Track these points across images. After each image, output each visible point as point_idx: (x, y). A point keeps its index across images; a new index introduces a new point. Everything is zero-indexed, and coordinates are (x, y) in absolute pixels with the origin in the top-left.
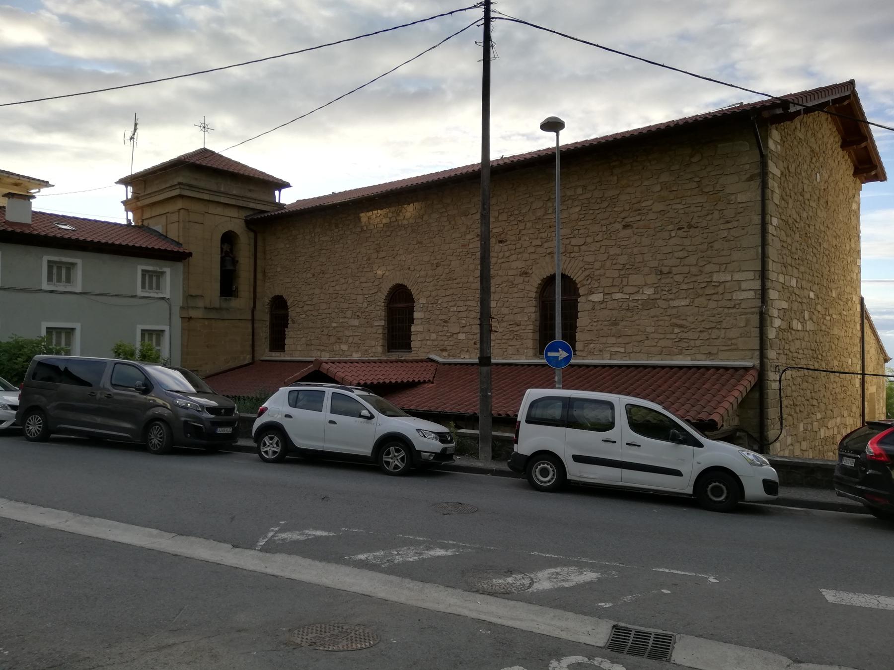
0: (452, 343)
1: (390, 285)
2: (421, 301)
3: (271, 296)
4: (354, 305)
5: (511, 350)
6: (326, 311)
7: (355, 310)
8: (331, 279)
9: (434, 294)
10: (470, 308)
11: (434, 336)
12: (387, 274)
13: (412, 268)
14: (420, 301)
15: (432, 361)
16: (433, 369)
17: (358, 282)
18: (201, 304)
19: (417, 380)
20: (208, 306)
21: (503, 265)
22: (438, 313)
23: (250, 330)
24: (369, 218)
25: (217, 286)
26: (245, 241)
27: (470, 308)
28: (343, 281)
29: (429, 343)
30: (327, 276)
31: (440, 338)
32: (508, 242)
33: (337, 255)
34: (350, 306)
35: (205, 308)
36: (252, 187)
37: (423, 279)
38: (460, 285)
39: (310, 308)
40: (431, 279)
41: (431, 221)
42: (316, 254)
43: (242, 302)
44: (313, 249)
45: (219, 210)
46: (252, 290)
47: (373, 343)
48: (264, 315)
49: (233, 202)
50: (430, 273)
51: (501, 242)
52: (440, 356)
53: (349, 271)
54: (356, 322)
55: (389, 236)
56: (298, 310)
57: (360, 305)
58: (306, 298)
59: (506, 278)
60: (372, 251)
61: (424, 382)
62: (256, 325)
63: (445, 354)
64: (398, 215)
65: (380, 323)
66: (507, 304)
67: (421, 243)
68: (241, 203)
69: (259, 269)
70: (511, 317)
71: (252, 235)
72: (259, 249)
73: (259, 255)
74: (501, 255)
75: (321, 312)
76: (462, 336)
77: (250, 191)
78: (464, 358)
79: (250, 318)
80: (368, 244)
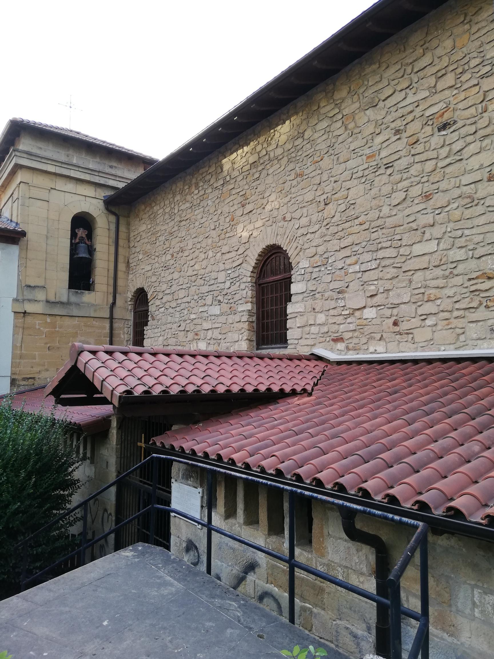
0: (352, 327)
1: (259, 250)
2: (301, 265)
3: (133, 290)
4: (214, 287)
5: (473, 331)
6: (185, 300)
7: (216, 293)
8: (190, 258)
9: (321, 250)
10: (383, 263)
11: (321, 318)
12: (255, 234)
13: (288, 217)
14: (301, 264)
15: (319, 358)
16: (317, 372)
17: (219, 254)
18: (41, 296)
19: (276, 389)
20: (52, 299)
21: (448, 170)
22: (329, 278)
23: (107, 330)
24: (233, 163)
25: (65, 276)
26: (103, 225)
27: (383, 263)
28: (202, 256)
29: (314, 329)
30: (186, 253)
31: (331, 320)
32: (460, 124)
33: (197, 224)
34: (211, 288)
35: (48, 302)
36: (114, 164)
37: (304, 231)
38: (366, 226)
39: (169, 298)
40: (317, 227)
41: (316, 135)
42: (176, 228)
43: (97, 298)
44: (173, 222)
45: (70, 187)
46: (111, 282)
47: (236, 337)
48: (125, 313)
49: (87, 177)
50: (314, 218)
51: (444, 126)
52: (332, 350)
53: (210, 241)
54: (216, 310)
55: (258, 179)
56: (158, 302)
57: (222, 286)
58: (164, 287)
59: (457, 192)
60: (236, 207)
61: (294, 393)
62: (115, 325)
63: (341, 346)
64: (269, 144)
65: (246, 307)
66: (462, 242)
67: (301, 175)
68: (97, 179)
69: (121, 259)
70: (473, 264)
71: (113, 218)
72: (122, 235)
73: (121, 242)
74: (444, 152)
75: (179, 301)
76: (369, 313)
77: (111, 167)
78: (375, 352)
79: (108, 315)
80: (232, 198)
